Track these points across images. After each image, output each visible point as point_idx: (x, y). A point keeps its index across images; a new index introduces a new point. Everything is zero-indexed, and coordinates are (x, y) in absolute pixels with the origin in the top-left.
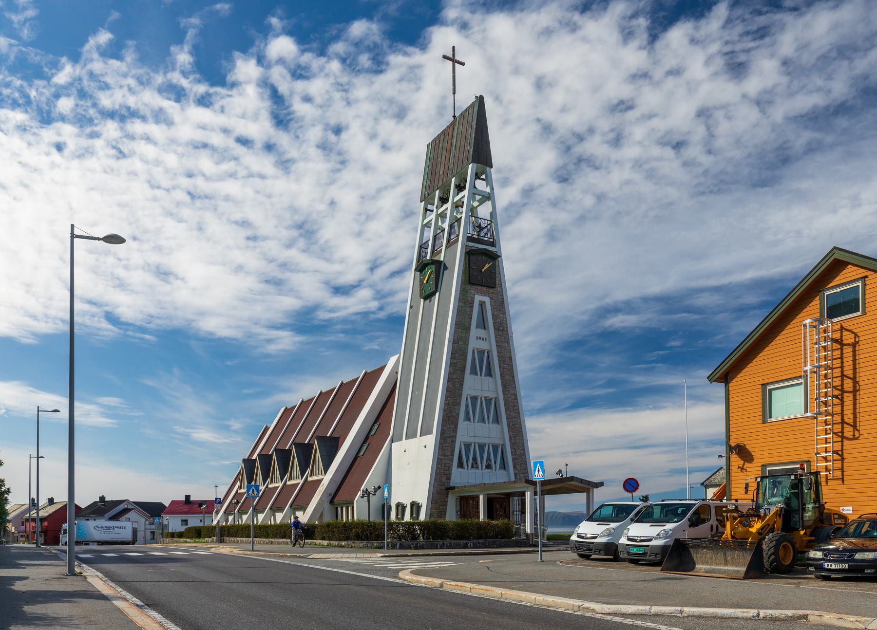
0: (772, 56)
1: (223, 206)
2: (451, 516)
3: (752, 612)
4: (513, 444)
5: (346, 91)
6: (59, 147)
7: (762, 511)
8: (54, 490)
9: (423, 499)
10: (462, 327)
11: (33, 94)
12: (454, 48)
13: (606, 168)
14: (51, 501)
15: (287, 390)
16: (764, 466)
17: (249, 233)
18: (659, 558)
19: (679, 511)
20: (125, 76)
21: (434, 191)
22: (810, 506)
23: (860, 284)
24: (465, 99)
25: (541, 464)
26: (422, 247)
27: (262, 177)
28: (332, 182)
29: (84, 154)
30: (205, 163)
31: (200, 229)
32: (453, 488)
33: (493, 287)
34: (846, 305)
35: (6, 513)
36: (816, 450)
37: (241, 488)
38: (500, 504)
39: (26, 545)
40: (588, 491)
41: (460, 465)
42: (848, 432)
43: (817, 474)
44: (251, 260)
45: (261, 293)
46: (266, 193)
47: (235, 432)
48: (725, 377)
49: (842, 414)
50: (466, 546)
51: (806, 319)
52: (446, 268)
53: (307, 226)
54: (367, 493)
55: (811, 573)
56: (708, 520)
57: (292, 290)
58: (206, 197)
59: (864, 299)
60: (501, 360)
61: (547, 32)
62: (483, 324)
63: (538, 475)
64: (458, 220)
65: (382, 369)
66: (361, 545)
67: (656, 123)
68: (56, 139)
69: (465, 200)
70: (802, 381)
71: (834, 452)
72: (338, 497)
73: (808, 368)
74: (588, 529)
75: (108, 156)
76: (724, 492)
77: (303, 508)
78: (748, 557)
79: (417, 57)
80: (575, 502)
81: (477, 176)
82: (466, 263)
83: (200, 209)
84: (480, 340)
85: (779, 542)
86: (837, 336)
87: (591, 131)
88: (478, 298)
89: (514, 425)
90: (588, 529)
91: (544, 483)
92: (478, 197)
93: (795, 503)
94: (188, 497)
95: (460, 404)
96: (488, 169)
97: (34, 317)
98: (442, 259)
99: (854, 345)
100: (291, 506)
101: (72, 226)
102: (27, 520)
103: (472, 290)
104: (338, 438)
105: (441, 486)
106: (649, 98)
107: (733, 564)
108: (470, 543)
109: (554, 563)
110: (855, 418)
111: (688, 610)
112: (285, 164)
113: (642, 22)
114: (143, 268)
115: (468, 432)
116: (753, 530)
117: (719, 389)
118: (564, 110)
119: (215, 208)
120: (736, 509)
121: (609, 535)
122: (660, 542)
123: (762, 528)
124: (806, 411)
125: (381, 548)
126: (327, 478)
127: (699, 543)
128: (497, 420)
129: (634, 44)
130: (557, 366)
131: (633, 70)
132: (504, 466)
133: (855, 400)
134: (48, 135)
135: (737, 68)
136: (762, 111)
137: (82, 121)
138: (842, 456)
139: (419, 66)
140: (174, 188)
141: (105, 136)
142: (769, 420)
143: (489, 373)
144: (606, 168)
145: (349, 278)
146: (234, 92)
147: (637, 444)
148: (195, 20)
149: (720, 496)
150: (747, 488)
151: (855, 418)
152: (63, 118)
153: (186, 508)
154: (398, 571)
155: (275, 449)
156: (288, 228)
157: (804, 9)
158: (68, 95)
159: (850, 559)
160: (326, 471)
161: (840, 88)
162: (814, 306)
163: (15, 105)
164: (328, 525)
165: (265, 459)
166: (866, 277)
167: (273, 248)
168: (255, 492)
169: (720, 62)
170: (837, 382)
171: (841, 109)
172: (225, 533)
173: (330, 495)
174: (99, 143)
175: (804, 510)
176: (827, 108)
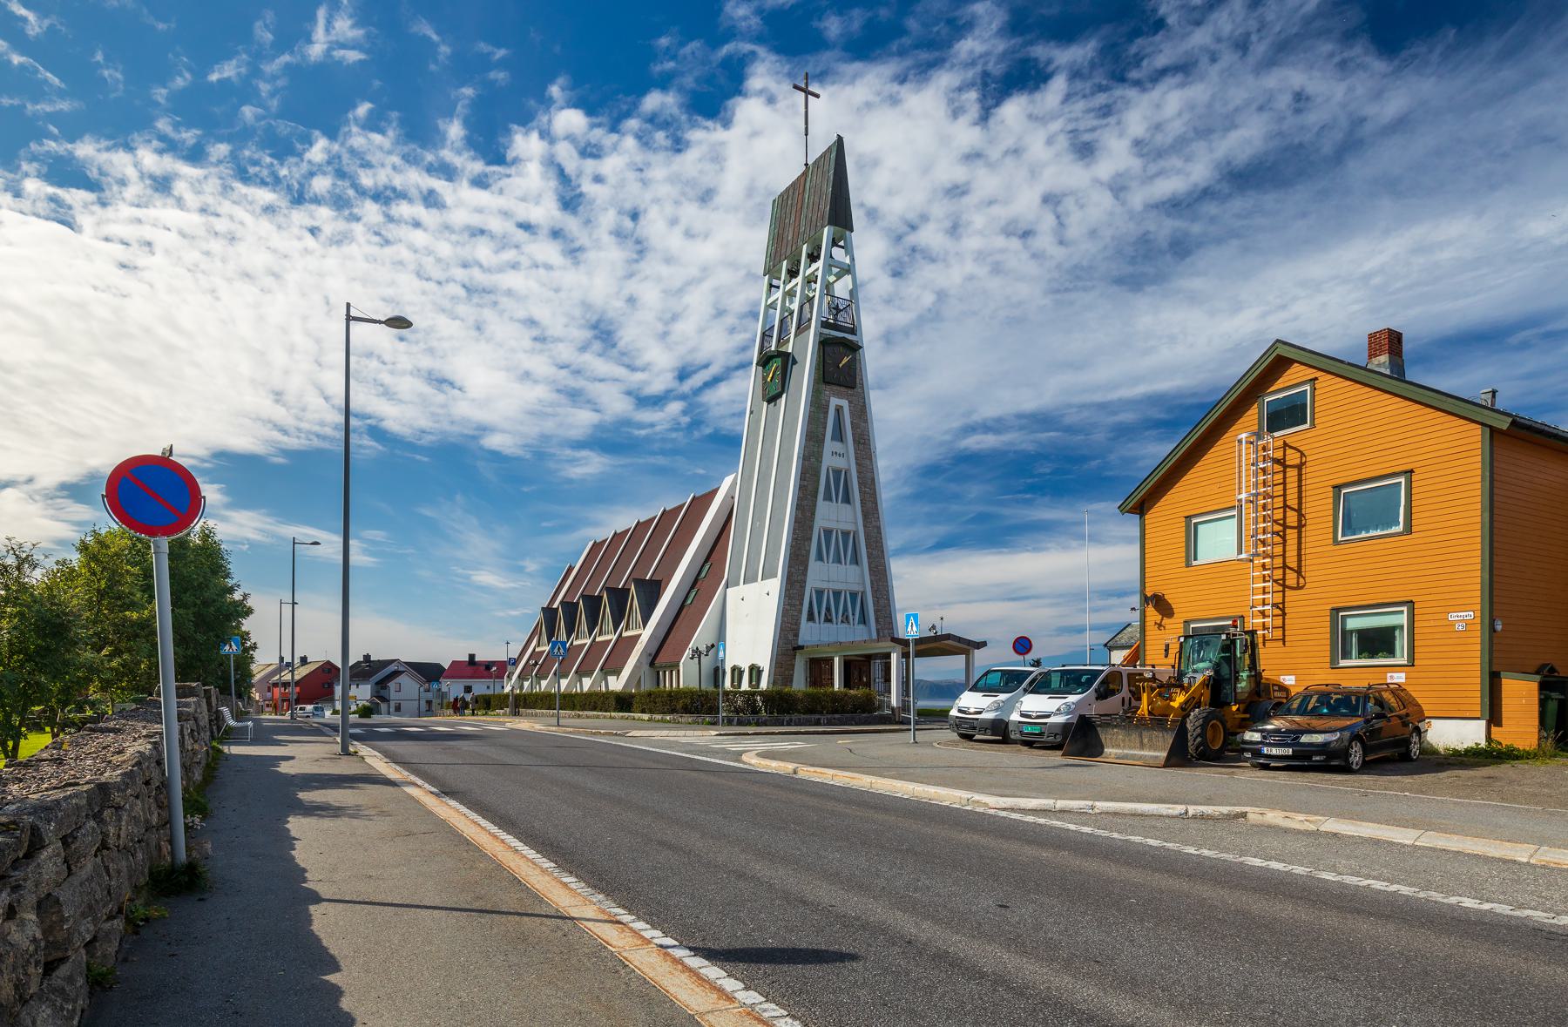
0: (1121, 135)
1: (504, 300)
3: (1179, 809)
4: (875, 592)
5: (641, 170)
6: (313, 231)
7: (1186, 681)
8: (320, 646)
9: (765, 663)
10: (814, 439)
11: (283, 172)
13: (944, 260)
14: (304, 661)
15: (596, 524)
16: (1187, 623)
17: (535, 332)
18: (1059, 739)
19: (1084, 679)
20: (390, 153)
21: (781, 262)
22: (1244, 675)
23: (1308, 388)
24: (819, 147)
25: (915, 616)
26: (766, 335)
27: (548, 267)
28: (630, 276)
29: (339, 240)
30: (483, 251)
31: (478, 328)
32: (802, 648)
34: (1290, 414)
35: (251, 676)
36: (1251, 601)
38: (857, 668)
39: (273, 717)
40: (967, 653)
41: (811, 618)
42: (1291, 578)
43: (1253, 633)
44: (540, 365)
45: (551, 405)
46: (556, 289)
47: (530, 575)
48: (1141, 507)
49: (1284, 556)
50: (818, 723)
51: (1242, 432)
52: (794, 362)
53: (602, 326)
54: (697, 653)
55: (1246, 760)
56: (1119, 691)
57: (589, 402)
58: (484, 290)
59: (1313, 408)
61: (868, 105)
62: (839, 435)
63: (911, 631)
64: (811, 300)
65: (715, 492)
67: (996, 210)
68: (309, 223)
69: (819, 274)
70: (1235, 512)
71: (1274, 605)
72: (660, 657)
73: (1243, 496)
74: (971, 701)
75: (369, 242)
76: (1137, 656)
77: (617, 673)
78: (1169, 739)
79: (720, 135)
80: (947, 667)
81: (834, 243)
83: (479, 305)
84: (836, 456)
85: (1206, 720)
86: (1279, 455)
87: (924, 218)
88: (834, 402)
90: (971, 701)
91: (919, 641)
92: (835, 270)
93: (1225, 670)
94: (472, 657)
97: (285, 432)
99: (1299, 467)
101: (348, 305)
102: (275, 685)
103: (827, 390)
105: (787, 646)
106: (986, 182)
107: (1152, 748)
108: (823, 718)
109: (930, 744)
110: (1300, 561)
111: (1102, 805)
112: (574, 253)
113: (973, 95)
114: (411, 374)
115: (820, 575)
116: (1175, 704)
117: (1131, 526)
118: (891, 192)
119: (495, 303)
120: (1154, 679)
121: (997, 710)
122: (1061, 719)
123: (1186, 702)
124: (1240, 552)
125: (714, 724)
126: (646, 634)
127: (1109, 721)
128: (856, 560)
129: (964, 121)
130: (917, 497)
131: (967, 150)
132: (864, 620)
133: (1300, 538)
134: (299, 217)
135: (1085, 150)
136: (1117, 197)
137: (339, 203)
138: (1283, 610)
139: (722, 144)
140: (447, 281)
141: (365, 220)
143: (847, 500)
144: (944, 260)
145: (657, 386)
146: (512, 170)
147: (1015, 594)
148: (468, 91)
149: (1133, 659)
150: (1167, 650)
151: (1300, 561)
152: (317, 200)
153: (470, 669)
154: (740, 753)
155: (582, 596)
156: (582, 327)
157: (1149, 85)
158: (324, 173)
159: (1295, 743)
161: (1199, 171)
162: (1252, 417)
163: (263, 183)
164: (650, 695)
165: (570, 608)
167: (566, 353)
169: (1063, 142)
170: (1278, 515)
171: (1206, 194)
172: (521, 703)
174: (358, 228)
175: (1237, 679)
176: (1190, 193)
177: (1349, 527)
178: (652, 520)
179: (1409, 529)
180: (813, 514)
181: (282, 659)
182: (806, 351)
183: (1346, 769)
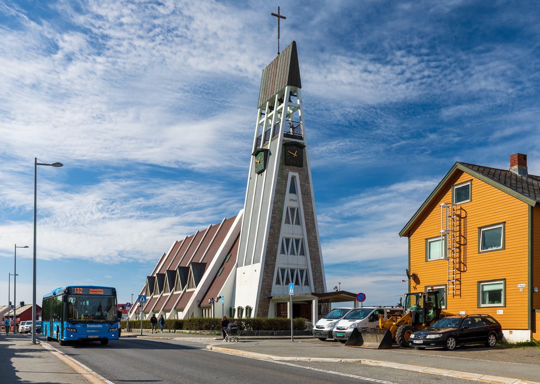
2: (271, 315)
10: (279, 193)
12: (279, 7)
14: (22, 304)
33: (301, 166)
50: (272, 335)
62: (293, 190)
66: (208, 333)
71: (456, 280)
81: (291, 94)
82: (282, 151)
88: (291, 174)
89: (314, 256)
95: (278, 243)
96: (298, 89)
98: (269, 148)
100: (175, 309)
101: (36, 159)
102: (7, 317)
103: (287, 168)
104: (206, 264)
105: (265, 295)
111: (313, 359)
126: (197, 290)
132: (307, 283)
138: (460, 282)
142: (429, 260)
143: (298, 223)
155: (179, 267)
160: (197, 283)
162: (449, 196)
165: (161, 276)
166: (472, 180)
168: (144, 300)
173: (199, 301)
177: (485, 246)
178: (182, 241)
179: (504, 248)
180: (279, 230)
181: (10, 303)
182: (275, 147)
183: (446, 349)
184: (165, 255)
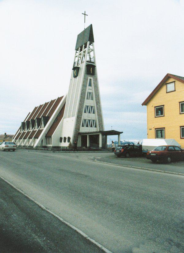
4: (99, 121)
10: (84, 86)
24: (87, 25)
37: (20, 131)
41: (83, 126)
60: (96, 95)
72: (48, 136)
81: (90, 44)
94: (5, 134)
95: (83, 108)
103: (88, 76)
132: (96, 127)
143: (92, 99)
160: (45, 125)
165: (28, 122)
184: (30, 113)
